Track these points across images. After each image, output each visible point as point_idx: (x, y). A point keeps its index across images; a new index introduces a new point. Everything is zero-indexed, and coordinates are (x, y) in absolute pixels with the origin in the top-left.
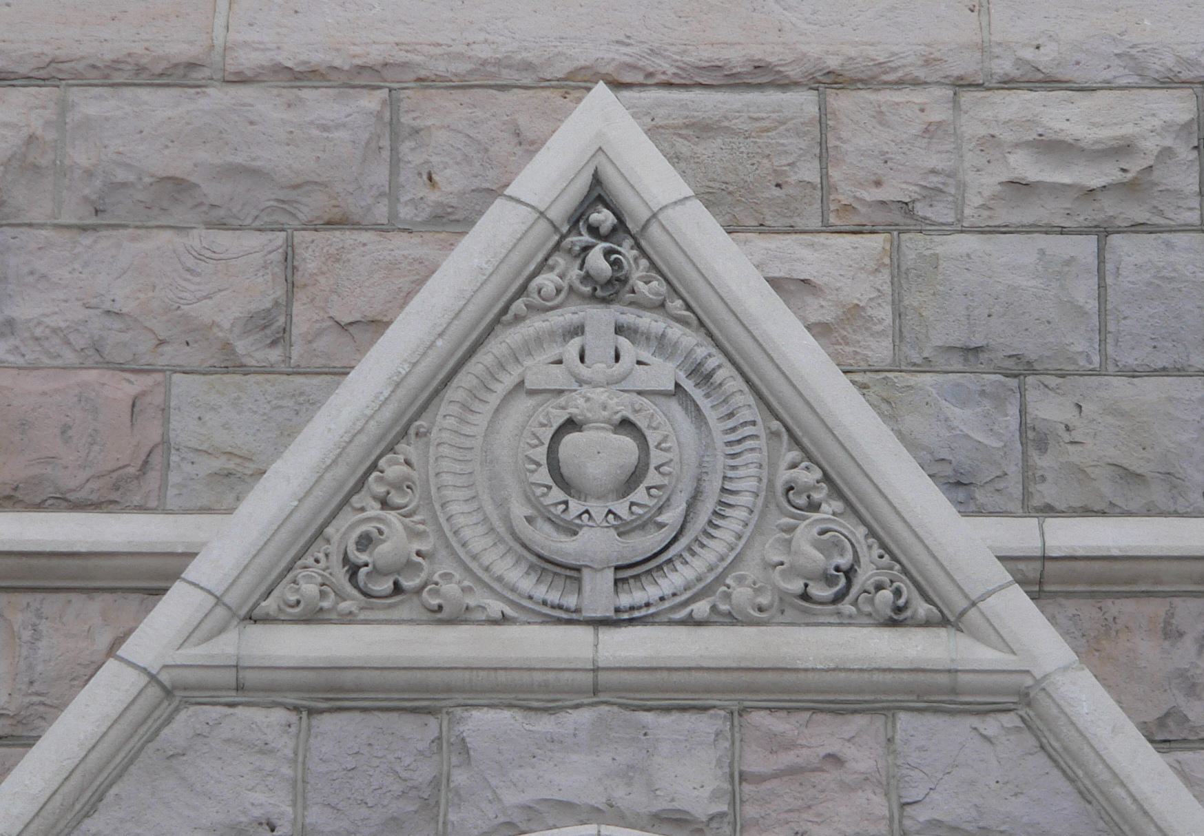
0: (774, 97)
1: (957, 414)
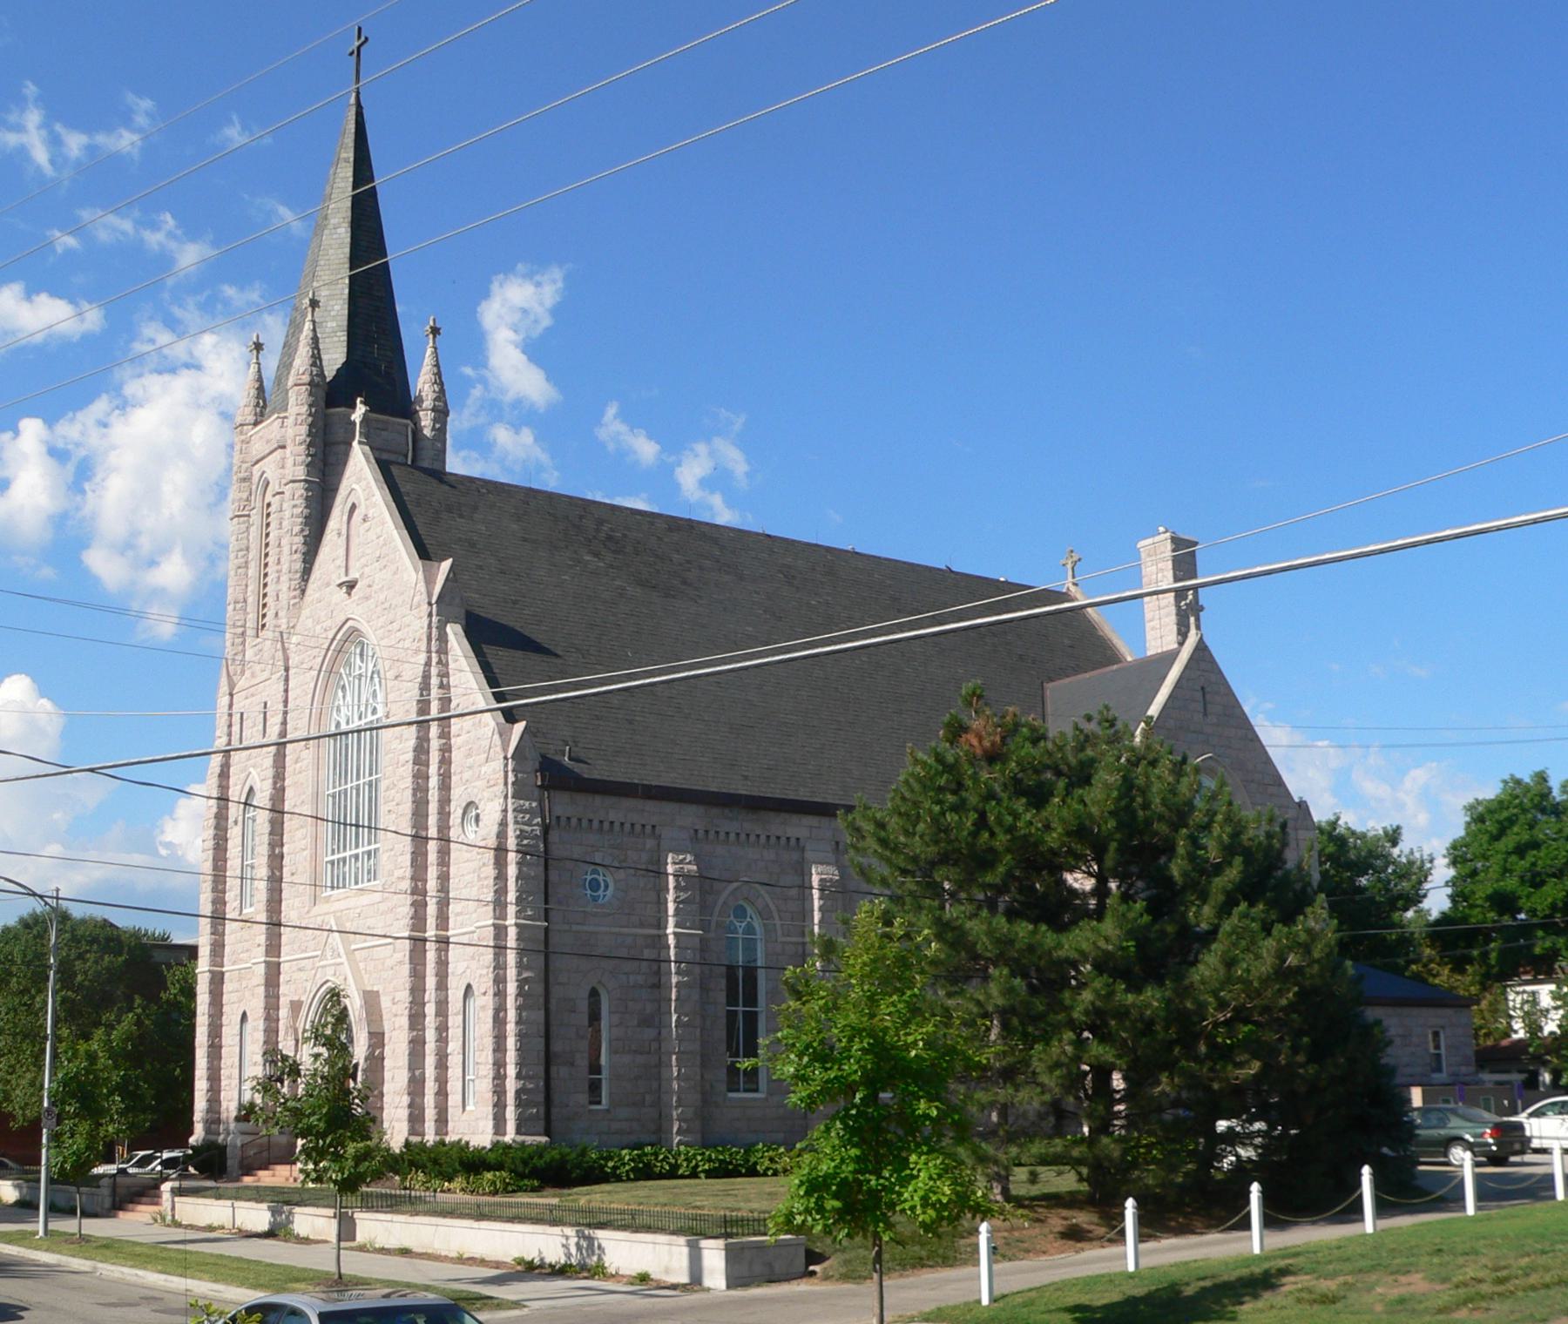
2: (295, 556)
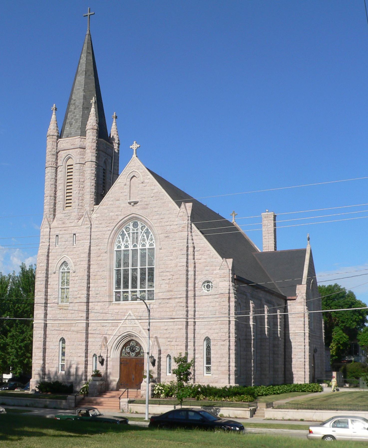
2: (92, 187)
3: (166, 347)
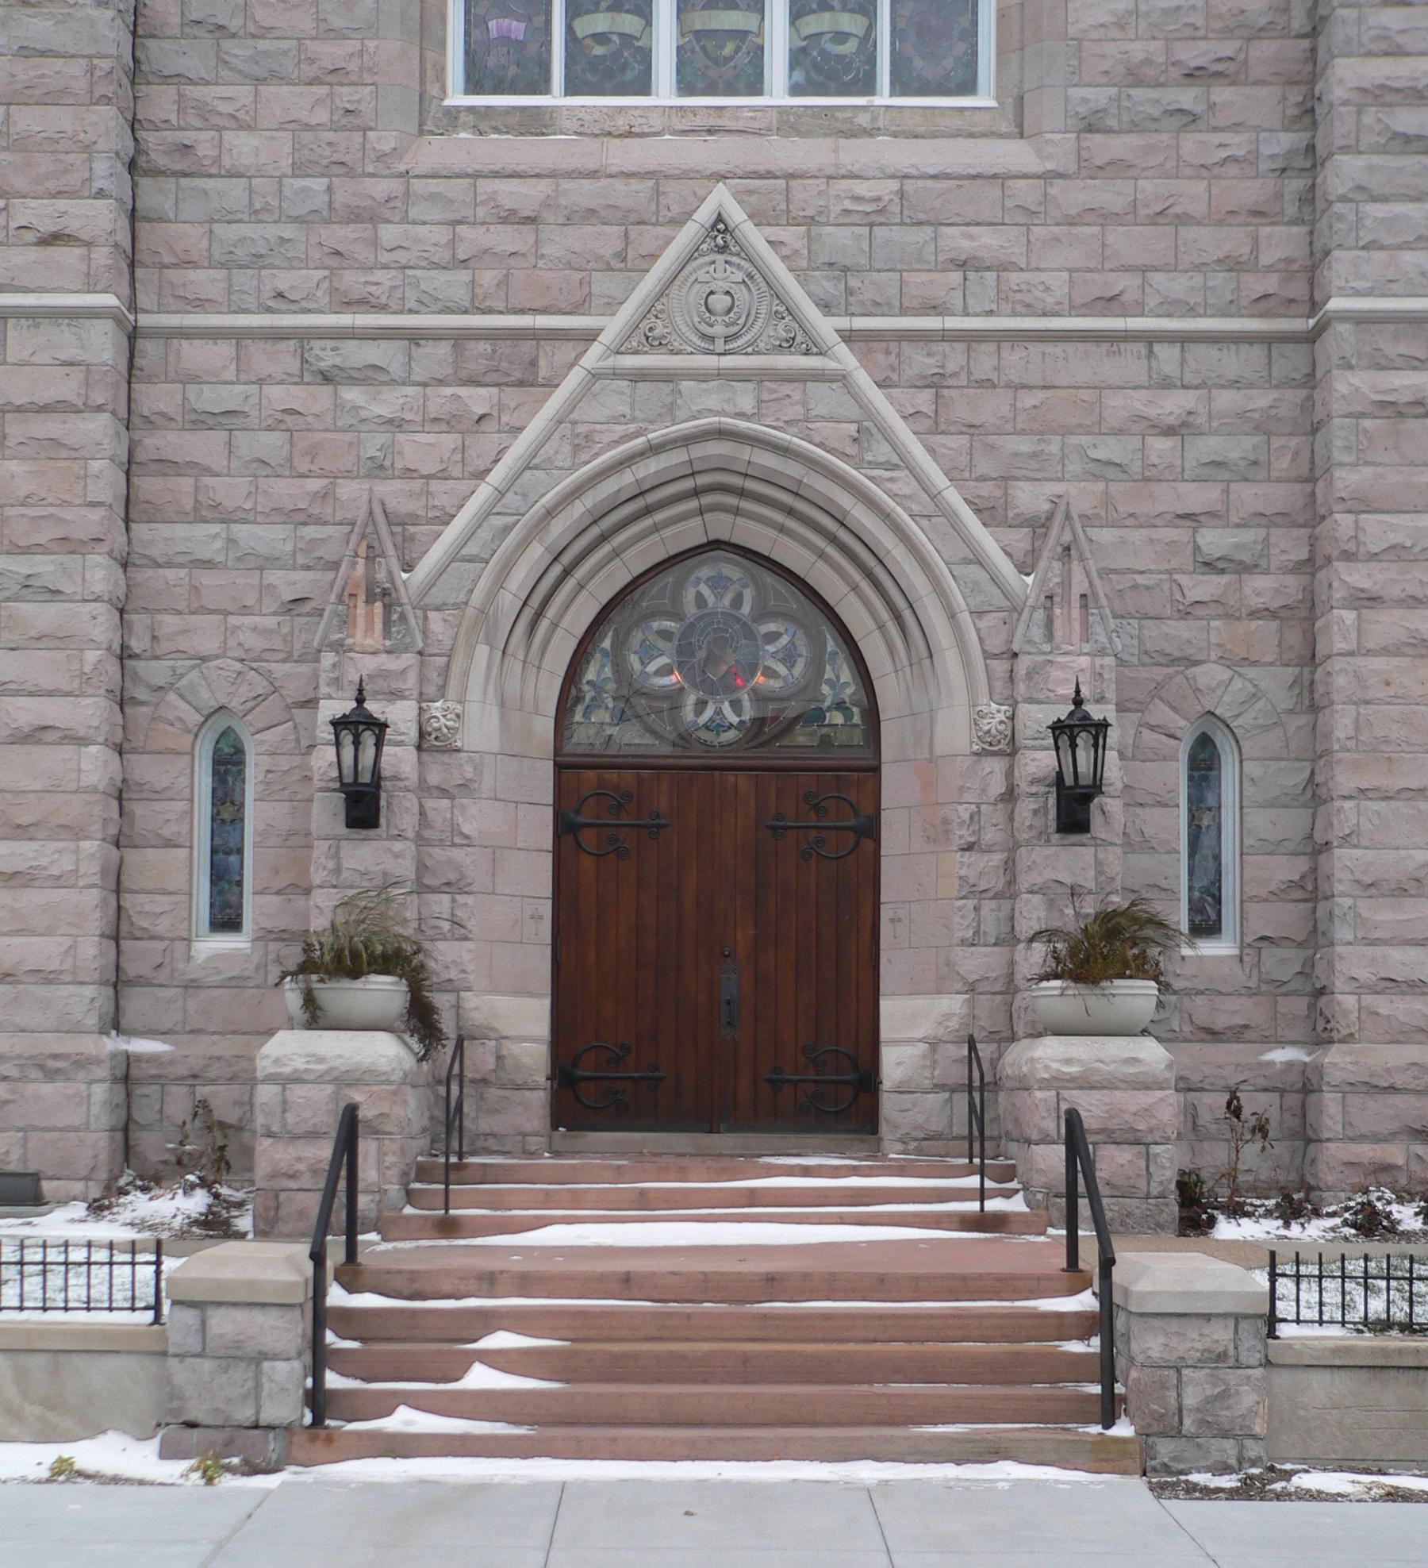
0: (773, 181)
1: (825, 283)
3: (1181, 630)
